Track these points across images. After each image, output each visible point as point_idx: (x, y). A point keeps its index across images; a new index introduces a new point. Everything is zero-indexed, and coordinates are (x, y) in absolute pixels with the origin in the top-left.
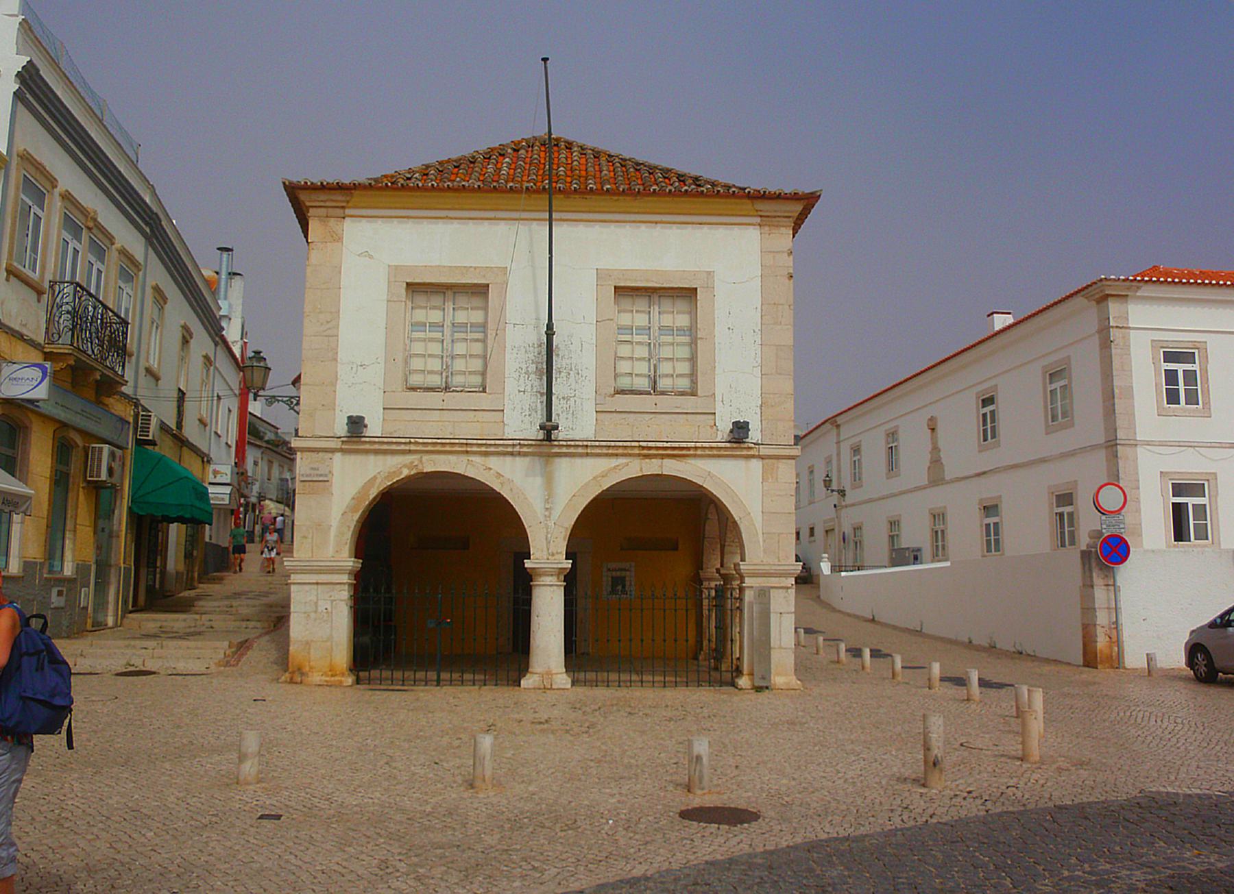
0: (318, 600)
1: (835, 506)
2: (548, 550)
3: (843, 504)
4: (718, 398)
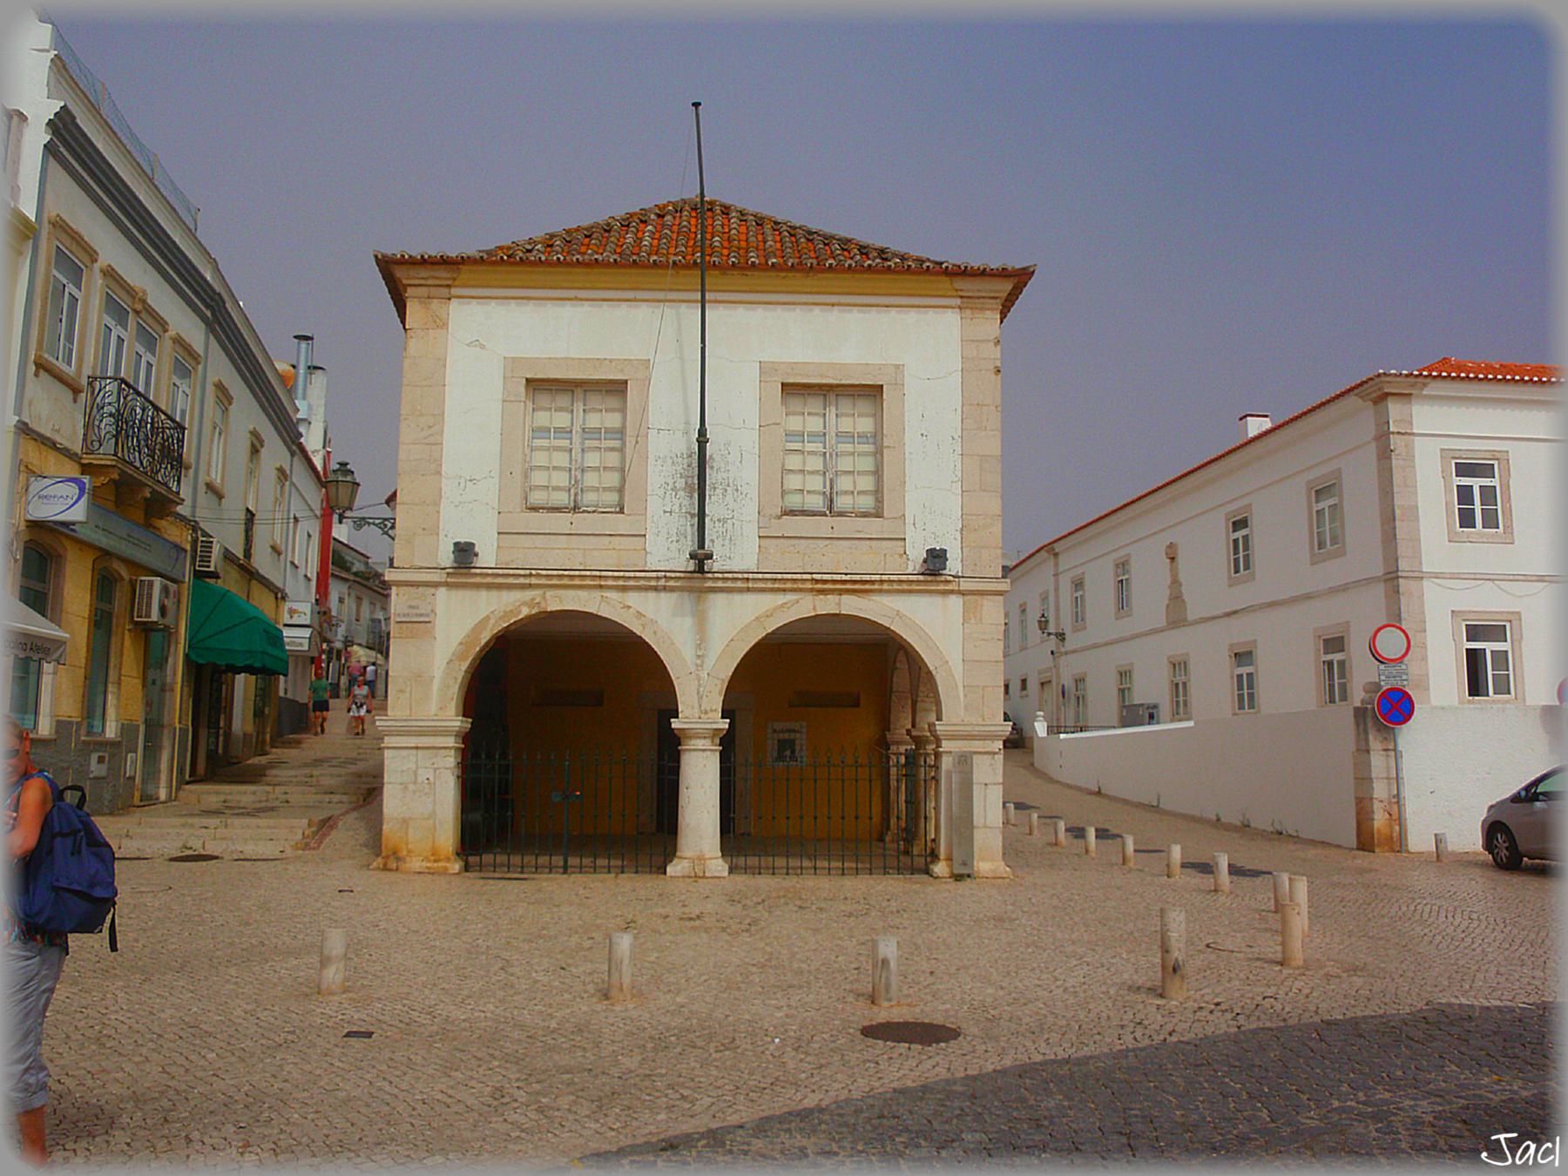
0: (417, 768)
1: (1052, 653)
3: (1063, 650)
4: (909, 520)
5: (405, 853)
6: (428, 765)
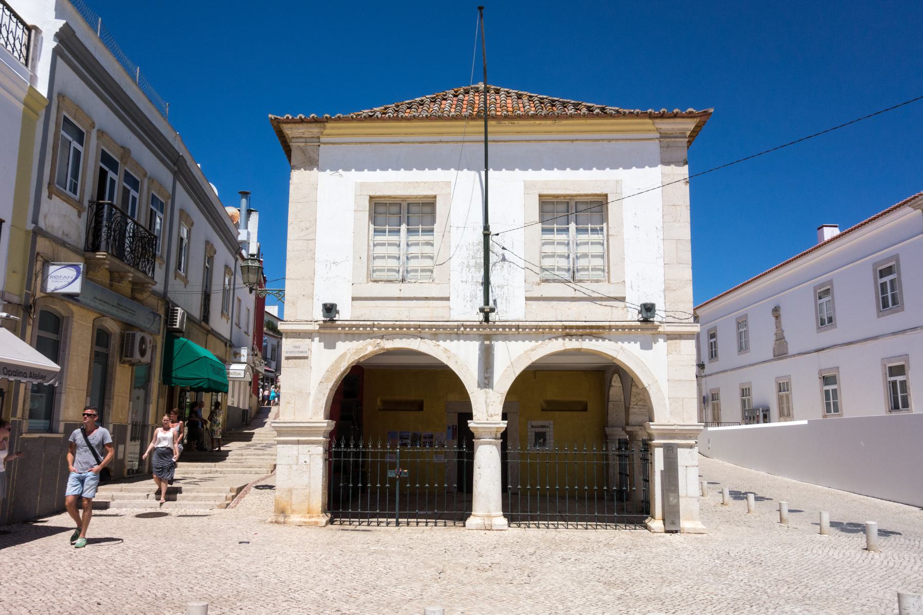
0: (298, 454)
2: (487, 412)
3: (703, 374)
4: (628, 284)
5: (290, 512)
6: (306, 452)
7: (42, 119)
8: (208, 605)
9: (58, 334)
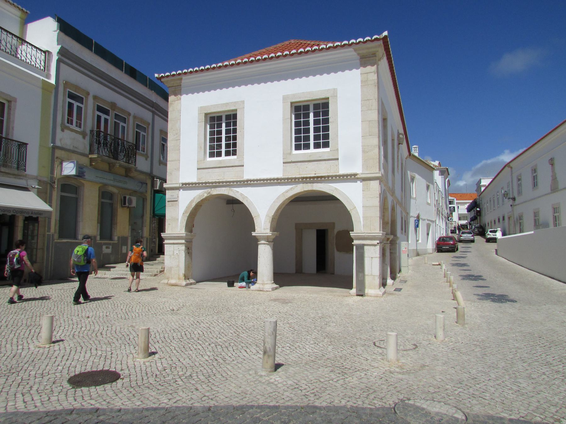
1: (511, 206)
3: (515, 204)
7: (53, 94)
8: (276, 322)
9: (77, 194)
